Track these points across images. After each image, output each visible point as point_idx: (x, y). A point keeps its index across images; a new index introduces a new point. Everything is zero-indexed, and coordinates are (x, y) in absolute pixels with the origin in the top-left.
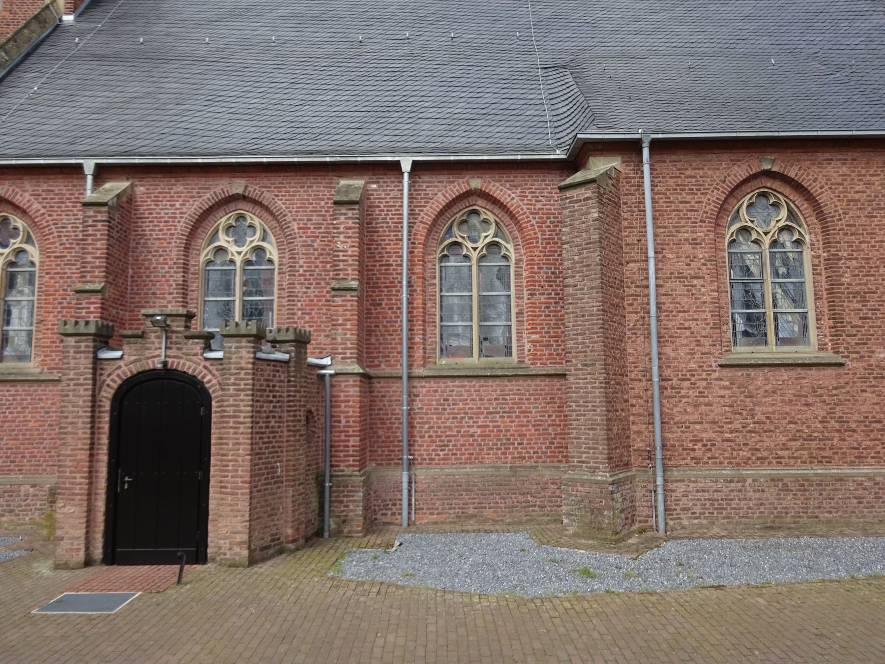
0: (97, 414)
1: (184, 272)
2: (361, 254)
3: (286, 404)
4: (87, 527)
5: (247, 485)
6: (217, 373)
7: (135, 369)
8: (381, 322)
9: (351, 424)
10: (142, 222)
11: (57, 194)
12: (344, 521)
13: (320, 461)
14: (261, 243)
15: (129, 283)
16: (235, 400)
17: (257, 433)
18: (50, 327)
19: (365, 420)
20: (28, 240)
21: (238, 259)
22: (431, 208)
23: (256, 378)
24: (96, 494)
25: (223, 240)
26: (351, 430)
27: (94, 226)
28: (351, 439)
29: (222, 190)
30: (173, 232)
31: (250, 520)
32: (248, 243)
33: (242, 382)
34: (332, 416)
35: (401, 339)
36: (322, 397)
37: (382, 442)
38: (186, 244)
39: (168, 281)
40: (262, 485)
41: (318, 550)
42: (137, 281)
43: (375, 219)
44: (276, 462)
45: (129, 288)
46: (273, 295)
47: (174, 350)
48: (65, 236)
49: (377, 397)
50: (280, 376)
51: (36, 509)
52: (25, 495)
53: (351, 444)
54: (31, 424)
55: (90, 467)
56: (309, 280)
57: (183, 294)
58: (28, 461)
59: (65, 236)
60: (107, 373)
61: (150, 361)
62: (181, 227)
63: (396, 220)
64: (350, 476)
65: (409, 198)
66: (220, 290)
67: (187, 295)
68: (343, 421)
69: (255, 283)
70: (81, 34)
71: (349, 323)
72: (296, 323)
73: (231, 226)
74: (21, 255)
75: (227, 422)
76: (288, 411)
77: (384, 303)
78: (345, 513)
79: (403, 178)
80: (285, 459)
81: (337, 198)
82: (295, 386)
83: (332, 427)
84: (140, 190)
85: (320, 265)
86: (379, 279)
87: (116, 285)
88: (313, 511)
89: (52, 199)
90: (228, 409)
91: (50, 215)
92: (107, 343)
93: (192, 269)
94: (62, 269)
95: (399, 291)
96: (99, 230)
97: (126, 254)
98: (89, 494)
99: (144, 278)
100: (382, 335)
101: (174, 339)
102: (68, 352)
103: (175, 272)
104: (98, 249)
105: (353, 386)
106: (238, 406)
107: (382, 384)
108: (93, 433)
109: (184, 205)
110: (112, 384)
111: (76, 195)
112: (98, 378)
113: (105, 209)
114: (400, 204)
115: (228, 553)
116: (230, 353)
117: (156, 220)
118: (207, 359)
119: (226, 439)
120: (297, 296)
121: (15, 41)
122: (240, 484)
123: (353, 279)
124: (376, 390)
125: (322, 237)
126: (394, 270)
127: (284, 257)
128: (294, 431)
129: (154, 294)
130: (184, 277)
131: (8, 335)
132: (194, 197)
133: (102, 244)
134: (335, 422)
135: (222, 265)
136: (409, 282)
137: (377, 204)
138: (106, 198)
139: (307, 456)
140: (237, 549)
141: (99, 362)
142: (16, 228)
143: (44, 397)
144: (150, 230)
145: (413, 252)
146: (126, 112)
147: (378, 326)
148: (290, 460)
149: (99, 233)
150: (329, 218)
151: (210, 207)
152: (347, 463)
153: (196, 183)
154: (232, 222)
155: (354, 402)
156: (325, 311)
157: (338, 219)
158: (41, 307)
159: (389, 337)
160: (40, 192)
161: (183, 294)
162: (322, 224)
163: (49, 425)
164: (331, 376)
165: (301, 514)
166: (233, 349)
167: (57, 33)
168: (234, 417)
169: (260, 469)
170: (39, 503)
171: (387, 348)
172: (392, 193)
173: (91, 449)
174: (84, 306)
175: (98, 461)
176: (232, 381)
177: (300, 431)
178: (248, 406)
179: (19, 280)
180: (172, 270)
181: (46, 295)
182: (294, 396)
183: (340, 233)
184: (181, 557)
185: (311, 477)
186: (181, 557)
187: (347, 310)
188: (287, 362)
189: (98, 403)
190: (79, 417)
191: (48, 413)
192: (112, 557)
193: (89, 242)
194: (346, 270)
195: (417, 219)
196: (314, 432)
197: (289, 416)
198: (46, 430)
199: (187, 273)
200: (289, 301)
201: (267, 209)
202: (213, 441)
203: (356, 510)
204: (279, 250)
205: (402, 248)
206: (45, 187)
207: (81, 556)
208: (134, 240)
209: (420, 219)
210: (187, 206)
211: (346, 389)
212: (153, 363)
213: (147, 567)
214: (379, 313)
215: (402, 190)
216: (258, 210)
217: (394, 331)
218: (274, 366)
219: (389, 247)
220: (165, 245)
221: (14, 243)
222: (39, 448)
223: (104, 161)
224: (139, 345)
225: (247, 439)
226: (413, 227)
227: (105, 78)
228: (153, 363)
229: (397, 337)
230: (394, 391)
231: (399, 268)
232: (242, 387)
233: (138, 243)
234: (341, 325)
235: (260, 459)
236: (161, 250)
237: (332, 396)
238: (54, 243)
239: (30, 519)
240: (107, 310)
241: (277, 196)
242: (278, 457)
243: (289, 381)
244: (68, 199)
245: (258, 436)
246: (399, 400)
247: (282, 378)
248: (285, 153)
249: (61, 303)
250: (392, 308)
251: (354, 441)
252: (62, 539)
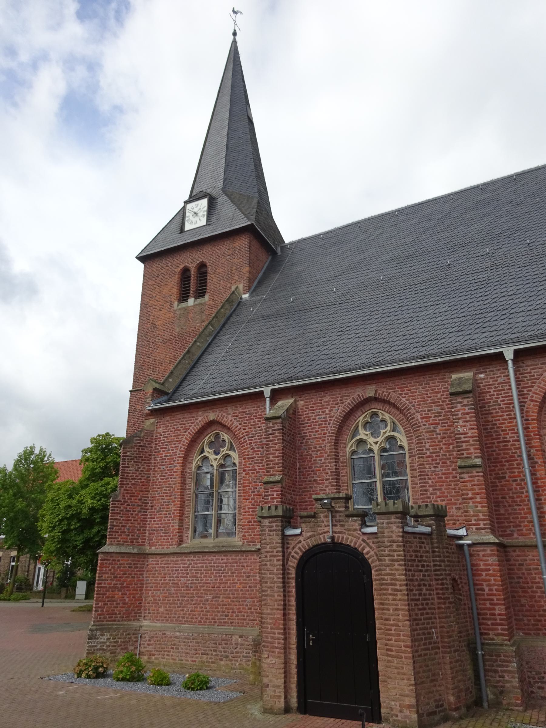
0: (286, 580)
1: (336, 462)
2: (480, 435)
3: (433, 573)
4: (285, 677)
5: (409, 650)
6: (373, 546)
7: (311, 543)
8: (508, 494)
9: (495, 592)
10: (304, 427)
11: (248, 414)
12: (501, 692)
13: (469, 628)
14: (392, 433)
15: (298, 474)
16: (391, 570)
17: (412, 600)
18: (247, 510)
19: (507, 588)
20: (231, 448)
21: (376, 448)
22: (539, 387)
23: (406, 549)
24: (290, 648)
25: (362, 434)
26: (495, 598)
27: (274, 434)
28: (497, 607)
29: (359, 395)
30: (325, 431)
31: (415, 685)
32: (381, 435)
33: (395, 554)
34: (475, 585)
35: (530, 509)
36: (463, 566)
37: (527, 611)
38: (335, 440)
39: (325, 470)
40: (422, 650)
41: (481, 721)
42: (303, 472)
43: (487, 403)
44: (431, 628)
45: (298, 477)
46: (407, 475)
47: (339, 527)
48: (254, 443)
49: (515, 565)
50: (425, 548)
51: (243, 656)
52: (236, 644)
53: (497, 612)
54: (238, 585)
55: (285, 624)
56: (436, 460)
57: (337, 479)
58: (237, 616)
59: (254, 443)
60: (291, 547)
61: (321, 537)
62: (331, 427)
63: (506, 402)
64: (501, 645)
65: (516, 381)
66: (364, 474)
67: (339, 479)
68: (487, 589)
69: (391, 467)
70: (254, 304)
71: (478, 496)
72: (429, 498)
73: (367, 422)
74: (227, 459)
75: (387, 590)
76: (436, 580)
77: (507, 476)
78: (501, 684)
79: (507, 365)
80: (438, 625)
81: (453, 390)
82: (439, 556)
83: (476, 595)
84: (301, 403)
85: (444, 447)
86: (499, 454)
87: (289, 476)
88: (470, 679)
89: (245, 417)
90: (386, 577)
91: (244, 429)
92: (289, 522)
93: (341, 459)
94: (253, 467)
95: (520, 464)
96: (277, 437)
97: (294, 452)
98: (285, 648)
99: (308, 469)
100: (510, 506)
101: (338, 518)
102: (265, 531)
103: (329, 463)
104: (276, 450)
105: (491, 555)
106: (394, 575)
107: (518, 553)
108: (284, 596)
109: (332, 410)
110: (295, 555)
111: (260, 413)
112: (285, 550)
113: (279, 421)
114: (508, 387)
115: (399, 714)
116: (383, 528)
117: (313, 424)
118: (364, 534)
119: (387, 604)
120: (427, 475)
121: (217, 318)
122: (403, 648)
123: (476, 457)
124: (512, 559)
125: (442, 423)
126: (512, 445)
127: (412, 443)
128: (444, 599)
129: (315, 480)
130: (336, 465)
131: (221, 517)
132: (338, 403)
133: (279, 447)
134: (478, 590)
135: (364, 454)
136: (529, 455)
137: (487, 390)
138: (280, 413)
139: (458, 623)
140: (407, 712)
141: (285, 538)
142: (224, 441)
143: (245, 564)
144: (309, 432)
145: (528, 428)
146: (286, 350)
147: (505, 498)
148: (443, 627)
149: (276, 439)
150: (446, 407)
151: (351, 410)
152: (496, 632)
153: (339, 393)
154: (368, 419)
155: (494, 570)
156: (453, 487)
157: (456, 407)
158: (241, 496)
159: (518, 508)
160: (238, 414)
161: (337, 479)
162: (442, 413)
163: (250, 587)
164: (469, 545)
165: (459, 681)
166: (385, 525)
167: (240, 307)
168: (392, 585)
169: (419, 634)
170: (245, 651)
171: (517, 518)
172: (499, 379)
173: (284, 609)
174: (270, 493)
175: (290, 620)
176: (387, 552)
177: (449, 598)
178: (402, 575)
179: (227, 477)
180: (327, 461)
181: (244, 487)
182: (440, 566)
183: (459, 419)
184: (362, 715)
185: (463, 644)
186: (362, 715)
187: (474, 485)
188: (429, 535)
189: (287, 571)
190: (275, 582)
191: (248, 577)
192: (304, 708)
193: (271, 445)
194: (469, 449)
195: (527, 398)
196: (460, 600)
197: (438, 584)
198: (248, 591)
199: (338, 462)
200: (421, 479)
201: (394, 405)
202: (376, 606)
203: (512, 682)
204: (407, 437)
205: (517, 426)
206: (241, 410)
207: (281, 704)
208: (299, 440)
209: (529, 398)
210: (334, 411)
211: (485, 558)
212: (324, 538)
213: (332, 719)
214: (505, 485)
215: (508, 375)
216: (387, 407)
217: (521, 501)
218: (420, 538)
219: (503, 426)
220: (321, 442)
221: (223, 451)
222: (243, 605)
223: (277, 387)
224: (312, 524)
225: (405, 605)
226: (524, 406)
227: (270, 330)
228: (324, 538)
229: (525, 507)
230: (530, 560)
231: (517, 443)
232: (396, 557)
233: (301, 443)
234: (471, 498)
235: (418, 624)
236: (318, 446)
237: (473, 565)
238: (247, 448)
239: (240, 664)
240: (285, 496)
241: (401, 394)
242: (433, 623)
243: (434, 552)
244: (254, 416)
245: (413, 603)
246: (538, 569)
247: (427, 549)
248: (403, 361)
249: (254, 492)
250: (516, 480)
251: (500, 609)
252: (268, 686)
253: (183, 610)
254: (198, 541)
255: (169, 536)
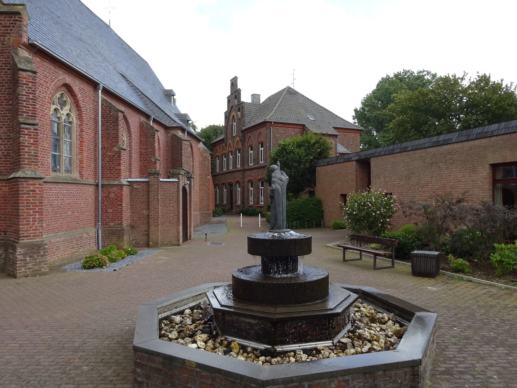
253: (56, 224)
254: (53, 174)
255: (45, 168)
